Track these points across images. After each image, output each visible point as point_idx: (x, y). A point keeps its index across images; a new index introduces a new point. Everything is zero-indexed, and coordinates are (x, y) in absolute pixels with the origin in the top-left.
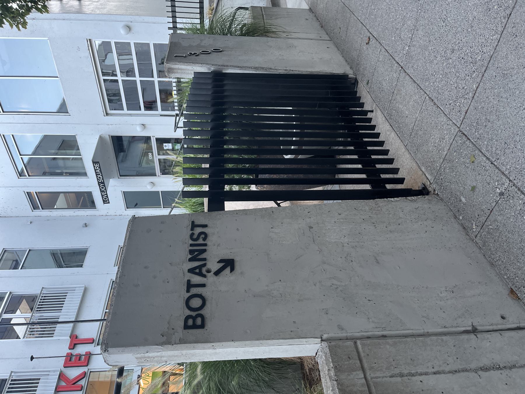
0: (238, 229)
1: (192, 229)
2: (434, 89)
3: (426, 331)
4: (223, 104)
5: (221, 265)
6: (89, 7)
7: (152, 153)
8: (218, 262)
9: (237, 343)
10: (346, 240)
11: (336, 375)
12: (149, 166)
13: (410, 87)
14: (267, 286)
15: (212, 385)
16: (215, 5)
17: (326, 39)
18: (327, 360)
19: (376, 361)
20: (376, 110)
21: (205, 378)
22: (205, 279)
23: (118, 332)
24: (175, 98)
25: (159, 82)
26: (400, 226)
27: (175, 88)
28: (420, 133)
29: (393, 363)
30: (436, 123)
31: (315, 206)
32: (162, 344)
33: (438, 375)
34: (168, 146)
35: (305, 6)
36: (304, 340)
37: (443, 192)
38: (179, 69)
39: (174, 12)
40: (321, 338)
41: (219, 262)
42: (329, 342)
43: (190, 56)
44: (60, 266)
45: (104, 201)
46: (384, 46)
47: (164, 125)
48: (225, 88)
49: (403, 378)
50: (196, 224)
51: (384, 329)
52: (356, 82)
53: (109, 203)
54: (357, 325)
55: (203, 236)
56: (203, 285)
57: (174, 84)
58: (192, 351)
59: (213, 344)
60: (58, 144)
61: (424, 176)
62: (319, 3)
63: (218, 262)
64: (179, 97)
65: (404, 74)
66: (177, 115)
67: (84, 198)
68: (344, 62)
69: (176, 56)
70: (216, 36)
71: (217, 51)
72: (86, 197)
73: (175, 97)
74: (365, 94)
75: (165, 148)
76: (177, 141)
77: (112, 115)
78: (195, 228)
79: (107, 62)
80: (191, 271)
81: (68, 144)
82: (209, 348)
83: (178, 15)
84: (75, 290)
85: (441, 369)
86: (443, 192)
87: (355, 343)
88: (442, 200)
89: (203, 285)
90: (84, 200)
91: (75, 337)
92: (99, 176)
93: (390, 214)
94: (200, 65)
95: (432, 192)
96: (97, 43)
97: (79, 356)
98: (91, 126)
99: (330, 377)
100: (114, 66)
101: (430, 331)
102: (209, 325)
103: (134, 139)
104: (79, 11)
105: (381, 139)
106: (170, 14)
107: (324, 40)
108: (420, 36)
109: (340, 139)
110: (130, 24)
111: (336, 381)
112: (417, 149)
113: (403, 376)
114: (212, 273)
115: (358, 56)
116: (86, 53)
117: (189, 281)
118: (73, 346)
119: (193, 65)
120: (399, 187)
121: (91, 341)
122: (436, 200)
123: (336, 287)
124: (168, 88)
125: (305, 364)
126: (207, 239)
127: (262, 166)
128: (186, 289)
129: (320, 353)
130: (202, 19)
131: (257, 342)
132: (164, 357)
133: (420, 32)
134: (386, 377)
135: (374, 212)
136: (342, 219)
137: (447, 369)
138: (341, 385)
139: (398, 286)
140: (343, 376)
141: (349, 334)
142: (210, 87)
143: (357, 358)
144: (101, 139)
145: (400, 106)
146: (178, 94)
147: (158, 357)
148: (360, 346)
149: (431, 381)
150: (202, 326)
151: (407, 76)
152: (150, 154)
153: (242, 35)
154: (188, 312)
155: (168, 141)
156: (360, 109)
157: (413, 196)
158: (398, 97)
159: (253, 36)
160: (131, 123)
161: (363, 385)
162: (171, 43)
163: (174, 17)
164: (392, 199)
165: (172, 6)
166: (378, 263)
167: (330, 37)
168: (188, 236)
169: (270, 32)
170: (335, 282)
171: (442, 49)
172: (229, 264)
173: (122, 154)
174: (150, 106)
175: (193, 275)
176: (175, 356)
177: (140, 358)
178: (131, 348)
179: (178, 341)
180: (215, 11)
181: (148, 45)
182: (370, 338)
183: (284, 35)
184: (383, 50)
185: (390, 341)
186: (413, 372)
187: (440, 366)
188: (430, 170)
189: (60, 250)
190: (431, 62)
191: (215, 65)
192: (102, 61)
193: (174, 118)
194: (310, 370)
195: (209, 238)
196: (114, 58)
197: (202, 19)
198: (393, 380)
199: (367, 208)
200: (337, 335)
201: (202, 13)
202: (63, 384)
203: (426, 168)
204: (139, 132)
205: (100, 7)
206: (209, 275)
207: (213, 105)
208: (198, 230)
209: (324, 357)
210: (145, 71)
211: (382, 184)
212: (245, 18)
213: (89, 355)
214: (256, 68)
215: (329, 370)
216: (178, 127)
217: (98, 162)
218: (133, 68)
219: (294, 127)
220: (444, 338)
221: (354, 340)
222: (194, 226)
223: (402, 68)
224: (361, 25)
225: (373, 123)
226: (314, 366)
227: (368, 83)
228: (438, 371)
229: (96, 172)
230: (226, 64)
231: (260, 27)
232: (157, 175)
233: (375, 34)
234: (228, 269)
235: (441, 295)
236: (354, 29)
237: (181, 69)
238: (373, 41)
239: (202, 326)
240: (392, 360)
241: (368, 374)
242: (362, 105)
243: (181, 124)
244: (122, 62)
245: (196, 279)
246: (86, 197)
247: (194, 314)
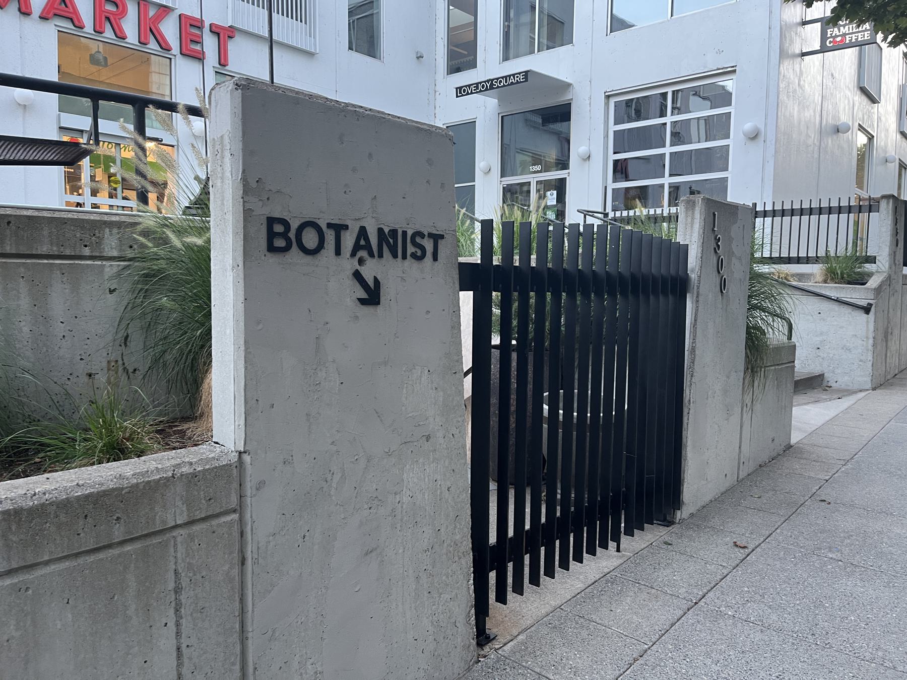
0: (428, 312)
1: (431, 235)
2: (661, 659)
3: (250, 635)
4: (635, 292)
5: (371, 283)
6: (791, 71)
7: (540, 172)
8: (375, 278)
9: (241, 307)
10: (406, 499)
11: (182, 475)
12: (518, 165)
13: (662, 616)
14: (334, 361)
15: (162, 264)
16: (794, 283)
17: (741, 472)
18: (208, 460)
19: (203, 546)
20: (621, 557)
21: (174, 250)
22: (348, 255)
23: (262, 105)
24: (641, 212)
25: (662, 186)
26: (426, 593)
27: (652, 212)
28: (584, 633)
29: (198, 577)
30: (602, 661)
31: (464, 447)
32: (245, 181)
33: (175, 654)
34: (551, 198)
35: (795, 438)
36: (242, 422)
37: (482, 671)
38: (693, 218)
39: (783, 213)
40: (245, 452)
41: (376, 281)
42: (237, 464)
43: (714, 239)
44: (351, 13)
45: (460, 88)
46: (733, 573)
47: (588, 193)
48: (661, 298)
49: (172, 592)
50: (439, 241)
51: (256, 562)
52: (668, 522)
53: (457, 96)
54: (263, 516)
55: (419, 253)
56: (338, 252)
57: (659, 211)
58: (230, 229)
59: (241, 265)
60: (558, 15)
61: (509, 638)
62: (802, 461)
63: (375, 278)
64: (643, 218)
65: (685, 607)
66: (606, 215)
67: (465, 56)
68: (703, 504)
69: (714, 215)
70: (747, 283)
71: (723, 285)
72: (468, 59)
73: (640, 211)
74: (647, 538)
75: (548, 193)
76: (561, 214)
77: (607, 105)
78: (432, 241)
79: (694, 100)
80: (363, 232)
81: (558, 31)
82: (234, 259)
83: (778, 219)
84: (310, 36)
85: (186, 660)
86: (482, 671)
87: (235, 511)
88: (469, 669)
89: (338, 252)
90: (462, 55)
91: (230, 34)
92: (504, 81)
93: (447, 577)
94: (700, 255)
95: (482, 652)
96: (729, 84)
97: (198, 41)
98: (588, 69)
99: (178, 466)
100: (688, 111)
101: (250, 642)
102: (273, 259)
103: (565, 141)
104: (783, 54)
105: (573, 564)
106: (778, 207)
107: (738, 469)
108: (752, 636)
109: (573, 495)
110: (761, 138)
111: (173, 477)
112: (555, 627)
113: (176, 592)
114: (358, 267)
115: (713, 528)
116: (712, 63)
117: (346, 227)
118: (216, 31)
119: (700, 244)
120: (492, 596)
121: (222, 61)
122: (469, 659)
123: (329, 479)
124: (650, 202)
125: (191, 425)
126: (413, 261)
127: (531, 357)
128: (333, 222)
129: (218, 449)
130: (771, 260)
131: (242, 342)
132: (222, 182)
133: (759, 636)
134: (176, 563)
135: (451, 549)
136: (441, 493)
137: (185, 671)
138: (165, 485)
139: (326, 588)
140: (179, 488)
141: (249, 500)
142: (663, 271)
143: (209, 513)
144: (567, 86)
145: (629, 600)
146: (649, 217)
147: (223, 173)
148: (228, 518)
149: (166, 642)
150: (271, 249)
151: (681, 613)
152: (538, 168)
153: (748, 327)
154: (294, 225)
155: (561, 198)
156: (622, 529)
157: (476, 619)
158: (644, 596)
159: (747, 346)
160: (592, 136)
161: (164, 522)
162: (734, 208)
163: (774, 213)
164: (472, 582)
165: (783, 210)
166: (366, 554)
167: (743, 479)
168: (419, 228)
169: (753, 377)
170: (337, 478)
171: (730, 673)
172: (372, 296)
173: (540, 121)
174: (621, 170)
175: (355, 236)
176: (223, 200)
177: (222, 143)
178: (240, 128)
179: (248, 206)
180: (784, 283)
181: (726, 169)
182: (242, 536)
183: (748, 400)
184: (725, 572)
185: (235, 572)
186: (183, 610)
187: (190, 659)
188: (521, 650)
189: (378, 13)
190: (708, 655)
191: (699, 281)
192: (696, 92)
193: (600, 210)
194: (182, 433)
195: (415, 264)
196: (700, 112)
197: (771, 260)
198: (171, 575)
199: (458, 537)
200: (248, 479)
201: (781, 260)
202: (152, 12)
203: (523, 643)
204: (577, 149)
205: (791, 90)
206: (355, 261)
207: (633, 276)
208: (428, 245)
209: (212, 455)
210: (681, 164)
211: (500, 563)
212: (775, 334)
213: (199, 57)
214: (693, 350)
215: (191, 464)
216: (585, 217)
217: (526, 81)
218: (684, 143)
219: (595, 413)
220: (237, 667)
221: (239, 509)
222: (436, 238)
223: (696, 603)
224: (768, 533)
225: (599, 550)
226: (190, 438)
227: (666, 543)
228: (182, 655)
229: (510, 76)
230: (701, 298)
231: (762, 359)
232: (503, 179)
233: (753, 557)
234: (364, 295)
235: (309, 663)
236: (760, 521)
237: (692, 223)
238: (740, 554)
239: (271, 249)
240: (204, 574)
241: (181, 531)
242: (629, 532)
243: (590, 220)
244: (694, 125)
245: (348, 240)
246: (468, 59)
247: (292, 235)
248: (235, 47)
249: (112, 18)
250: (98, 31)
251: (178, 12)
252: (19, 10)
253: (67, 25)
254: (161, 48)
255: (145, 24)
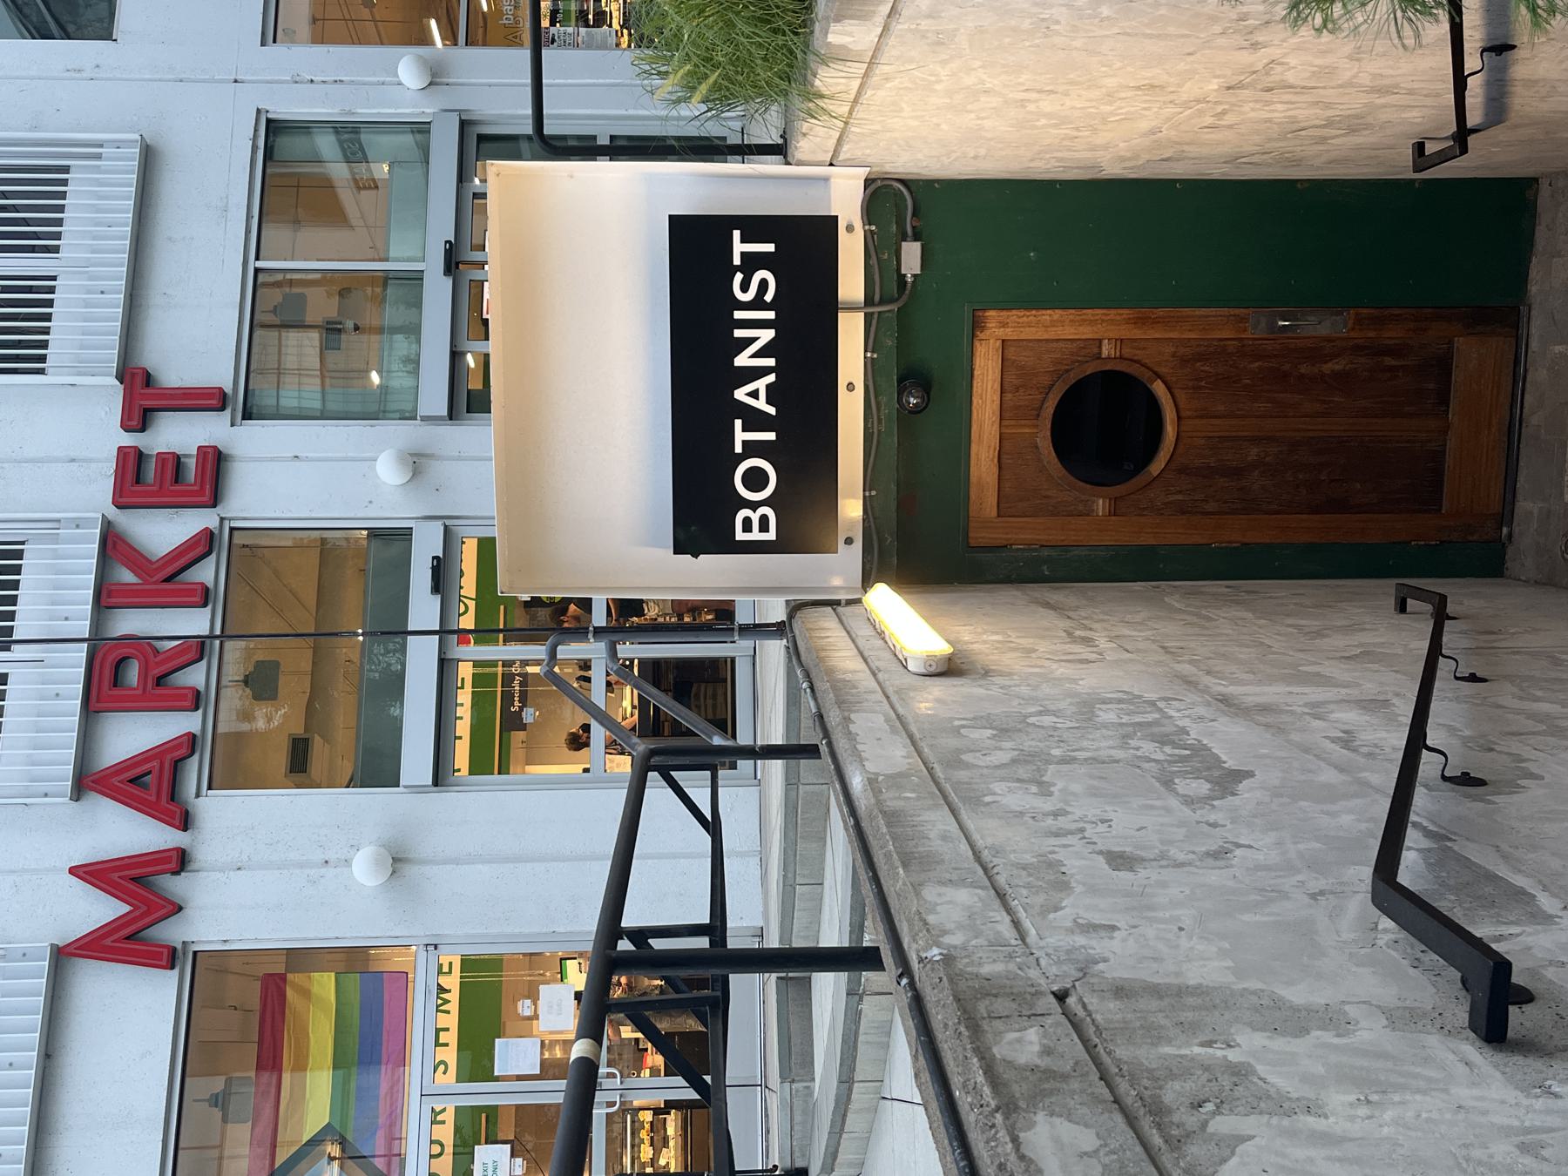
84: (99, 157)
91: (139, 381)
97: (174, 462)
118: (106, 598)
202: (127, 576)
213: (215, 462)
248: (175, 372)
249: (157, 672)
250: (195, 700)
251: (112, 512)
252: (176, 873)
253: (193, 773)
254: (209, 553)
255: (158, 593)
